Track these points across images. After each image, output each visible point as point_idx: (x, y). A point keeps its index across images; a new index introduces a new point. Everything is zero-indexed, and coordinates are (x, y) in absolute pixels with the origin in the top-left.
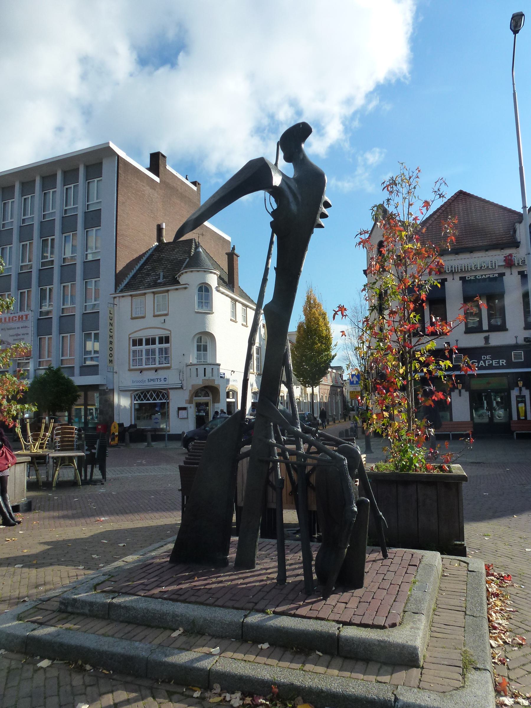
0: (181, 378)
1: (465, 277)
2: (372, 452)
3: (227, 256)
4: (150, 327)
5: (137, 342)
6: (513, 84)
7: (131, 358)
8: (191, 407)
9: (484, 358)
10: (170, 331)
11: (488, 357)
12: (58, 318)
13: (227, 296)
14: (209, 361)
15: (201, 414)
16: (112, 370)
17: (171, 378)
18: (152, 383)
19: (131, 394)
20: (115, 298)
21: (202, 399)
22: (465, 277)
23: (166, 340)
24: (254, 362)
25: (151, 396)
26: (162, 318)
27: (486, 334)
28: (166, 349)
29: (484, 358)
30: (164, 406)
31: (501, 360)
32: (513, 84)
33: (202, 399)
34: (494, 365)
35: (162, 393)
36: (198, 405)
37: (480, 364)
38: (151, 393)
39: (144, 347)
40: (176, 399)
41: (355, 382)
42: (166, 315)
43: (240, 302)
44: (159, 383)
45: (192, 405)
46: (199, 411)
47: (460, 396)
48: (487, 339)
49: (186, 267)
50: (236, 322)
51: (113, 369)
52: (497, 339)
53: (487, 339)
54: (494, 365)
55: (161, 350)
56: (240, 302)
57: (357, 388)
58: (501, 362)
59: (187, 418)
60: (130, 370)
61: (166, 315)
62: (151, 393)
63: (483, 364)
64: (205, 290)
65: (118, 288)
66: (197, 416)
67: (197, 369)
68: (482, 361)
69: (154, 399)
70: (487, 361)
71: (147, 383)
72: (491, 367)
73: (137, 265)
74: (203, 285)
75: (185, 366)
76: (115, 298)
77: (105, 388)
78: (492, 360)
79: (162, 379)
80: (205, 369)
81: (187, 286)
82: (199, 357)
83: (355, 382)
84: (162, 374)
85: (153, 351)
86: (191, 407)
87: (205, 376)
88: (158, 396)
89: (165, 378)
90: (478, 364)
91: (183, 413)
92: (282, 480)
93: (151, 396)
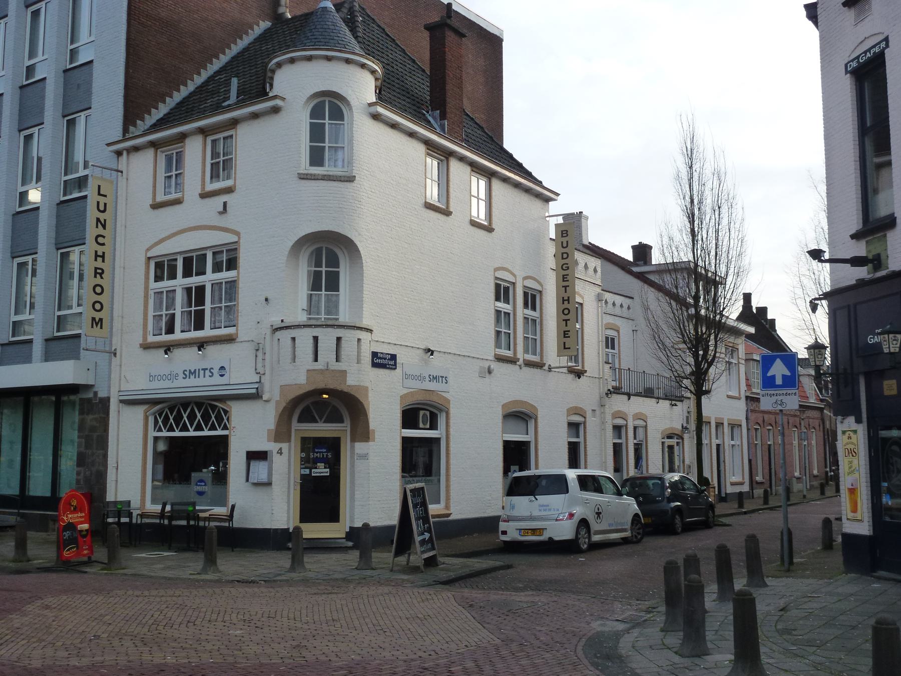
0: (259, 365)
3: (426, 34)
4: (191, 225)
5: (163, 268)
7: (151, 313)
8: (280, 452)
10: (237, 234)
12: (10, 218)
13: (412, 135)
14: (344, 316)
15: (316, 472)
16: (107, 349)
17: (233, 366)
18: (192, 381)
19: (145, 413)
20: (119, 153)
21: (322, 429)
23: (229, 259)
25: (192, 417)
26: (219, 200)
28: (158, 278)
30: (217, 451)
33: (322, 429)
35: (211, 408)
36: (309, 445)
38: (192, 410)
39: (180, 282)
40: (248, 428)
41: (779, 381)
42: (229, 190)
43: (462, 159)
44: (207, 381)
45: (285, 446)
46: (308, 462)
49: (786, 351)
50: (447, 213)
51: (111, 344)
55: (216, 285)
56: (462, 159)
57: (786, 399)
59: (269, 484)
60: (146, 347)
61: (229, 190)
62: (192, 410)
64: (329, 107)
65: (131, 128)
66: (303, 477)
67: (294, 339)
69: (199, 428)
71: (181, 382)
73: (199, 74)
74: (327, 99)
75: (269, 332)
76: (119, 153)
77: (91, 395)
79: (216, 371)
80: (339, 339)
81: (278, 102)
82: (311, 308)
83: (779, 381)
84: (216, 355)
85: (201, 290)
86: (280, 452)
87: (316, 360)
88: (206, 417)
89: (222, 368)
91: (260, 470)
93: (192, 417)
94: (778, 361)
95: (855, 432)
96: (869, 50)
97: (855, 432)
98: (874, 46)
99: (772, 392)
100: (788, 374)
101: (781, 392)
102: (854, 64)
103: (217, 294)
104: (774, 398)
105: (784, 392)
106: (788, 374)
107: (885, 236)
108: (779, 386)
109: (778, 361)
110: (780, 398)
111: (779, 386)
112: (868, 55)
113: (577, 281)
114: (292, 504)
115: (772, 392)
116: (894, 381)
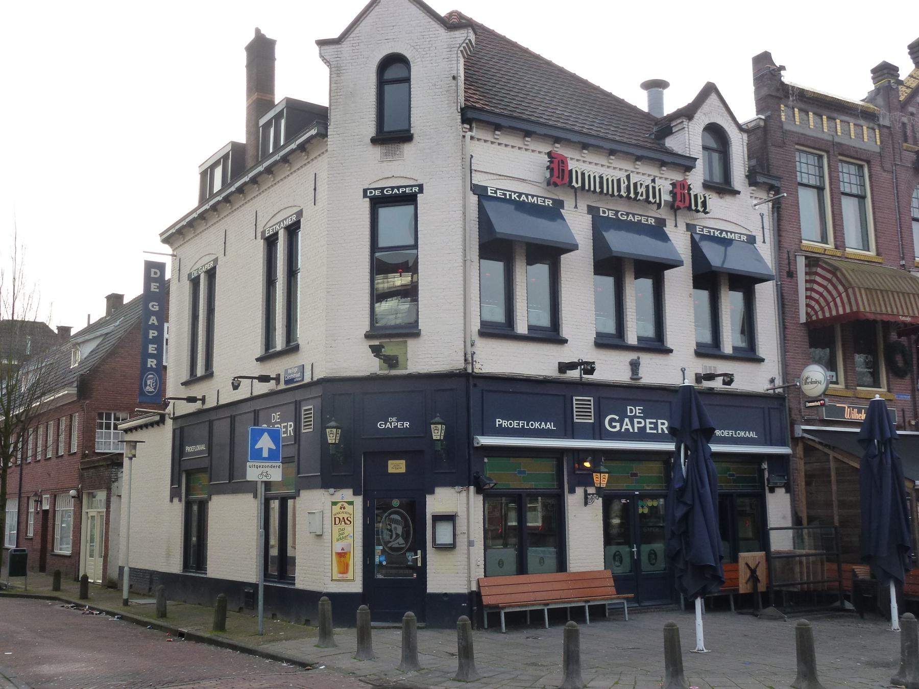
1: (598, 208)
2: (371, 657)
6: (315, 189)
9: (631, 411)
11: (638, 410)
22: (598, 208)
24: (766, 231)
27: (633, 356)
29: (631, 411)
31: (660, 421)
32: (315, 189)
34: (648, 431)
37: (624, 427)
41: (265, 454)
47: (89, 316)
48: (635, 366)
52: (657, 372)
53: (635, 366)
54: (648, 431)
58: (660, 426)
63: (630, 427)
68: (627, 420)
70: (636, 420)
72: (642, 435)
78: (644, 418)
83: (265, 454)
90: (621, 426)
92: (169, 281)
94: (266, 435)
95: (351, 503)
96: (398, 188)
97: (351, 503)
98: (405, 187)
99: (259, 464)
100: (274, 447)
101: (267, 464)
102: (377, 193)
103: (871, 301)
104: (260, 470)
105: (270, 464)
106: (274, 447)
107: (406, 342)
108: (265, 459)
109: (266, 435)
110: (266, 470)
111: (265, 459)
112: (396, 191)
113: (91, 323)
114: (888, 429)
115: (259, 464)
116: (403, 462)
